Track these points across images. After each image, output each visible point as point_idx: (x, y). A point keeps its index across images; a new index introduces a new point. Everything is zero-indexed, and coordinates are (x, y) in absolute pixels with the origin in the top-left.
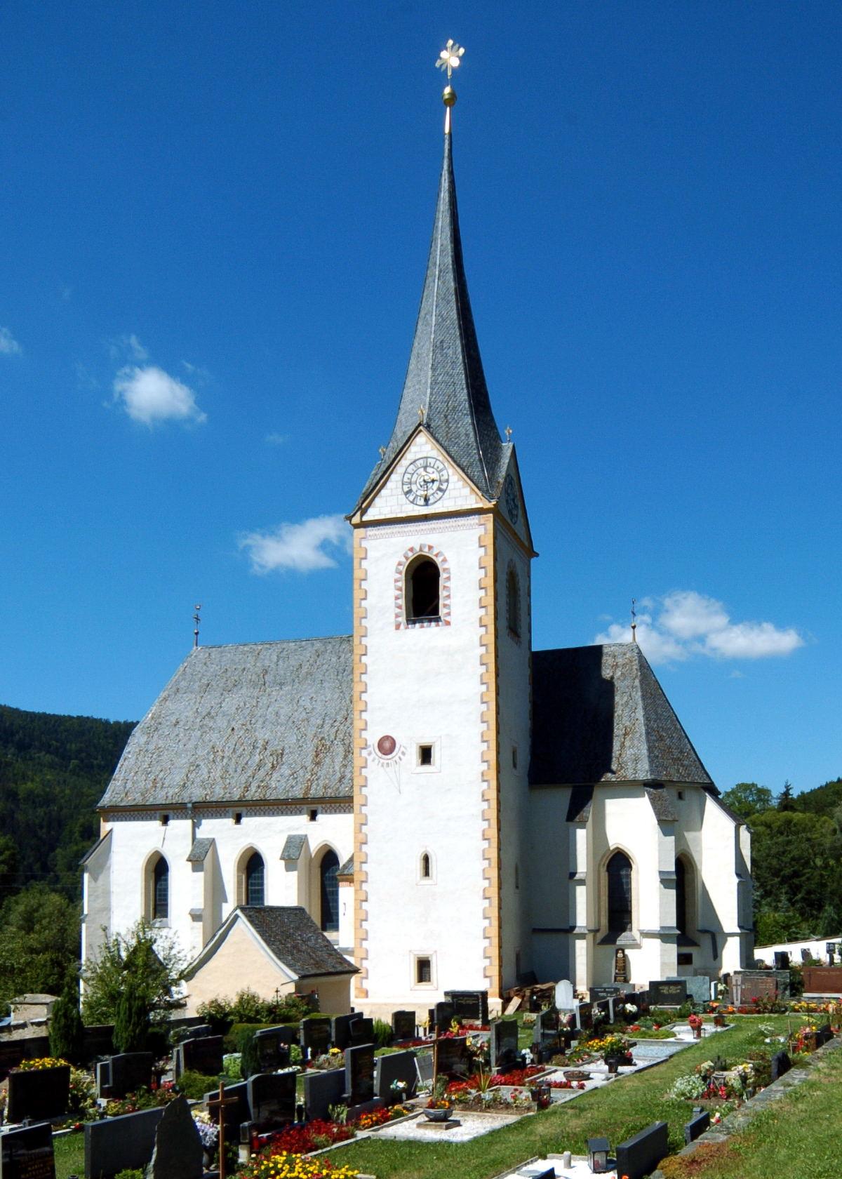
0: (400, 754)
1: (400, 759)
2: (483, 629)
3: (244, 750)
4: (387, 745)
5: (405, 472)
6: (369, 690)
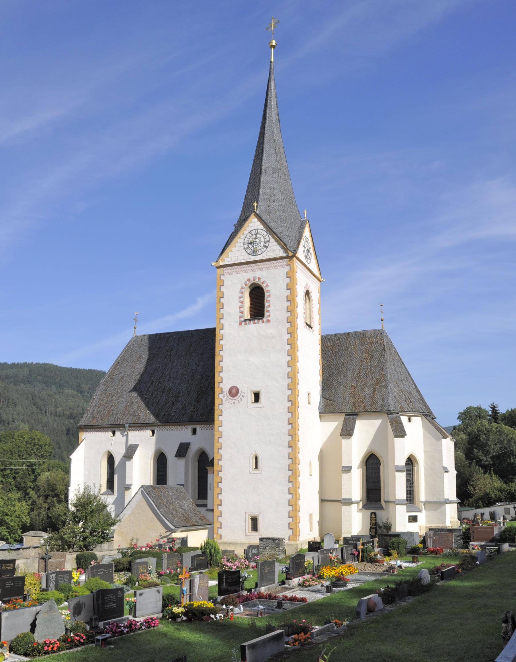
0: (241, 397)
1: (241, 399)
4: (234, 391)
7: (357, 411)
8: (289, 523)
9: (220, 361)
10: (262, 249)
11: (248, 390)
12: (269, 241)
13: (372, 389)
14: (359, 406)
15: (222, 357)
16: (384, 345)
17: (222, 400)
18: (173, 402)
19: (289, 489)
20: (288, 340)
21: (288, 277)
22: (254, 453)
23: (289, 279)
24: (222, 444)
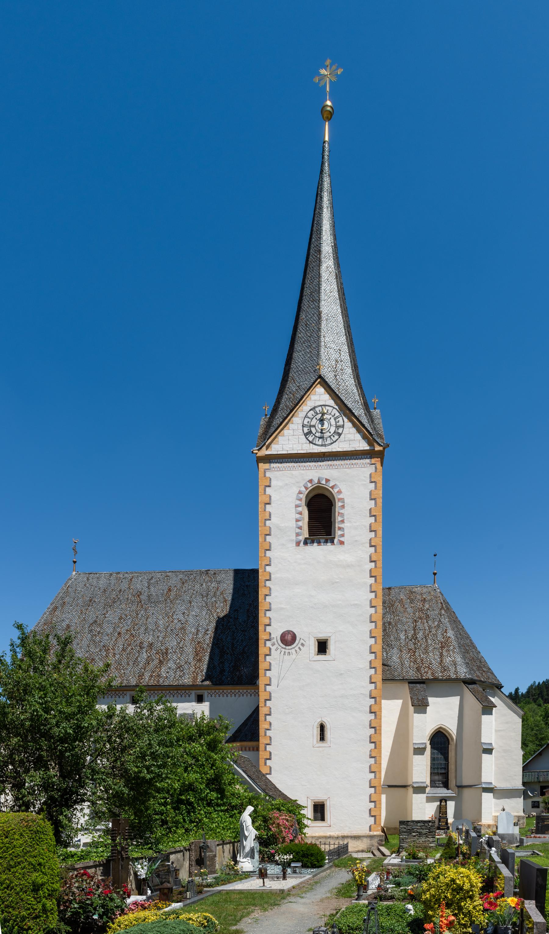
0: (300, 645)
1: (299, 648)
2: (373, 549)
3: (132, 649)
4: (289, 637)
5: (305, 417)
6: (273, 594)
7: (424, 678)
8: (370, 810)
9: (267, 595)
10: (332, 437)
11: (310, 636)
12: (343, 426)
13: (438, 653)
14: (427, 673)
15: (270, 589)
16: (441, 603)
17: (270, 649)
18: (160, 661)
19: (370, 767)
20: (371, 571)
21: (372, 482)
22: (319, 720)
23: (373, 484)
24: (270, 708)
